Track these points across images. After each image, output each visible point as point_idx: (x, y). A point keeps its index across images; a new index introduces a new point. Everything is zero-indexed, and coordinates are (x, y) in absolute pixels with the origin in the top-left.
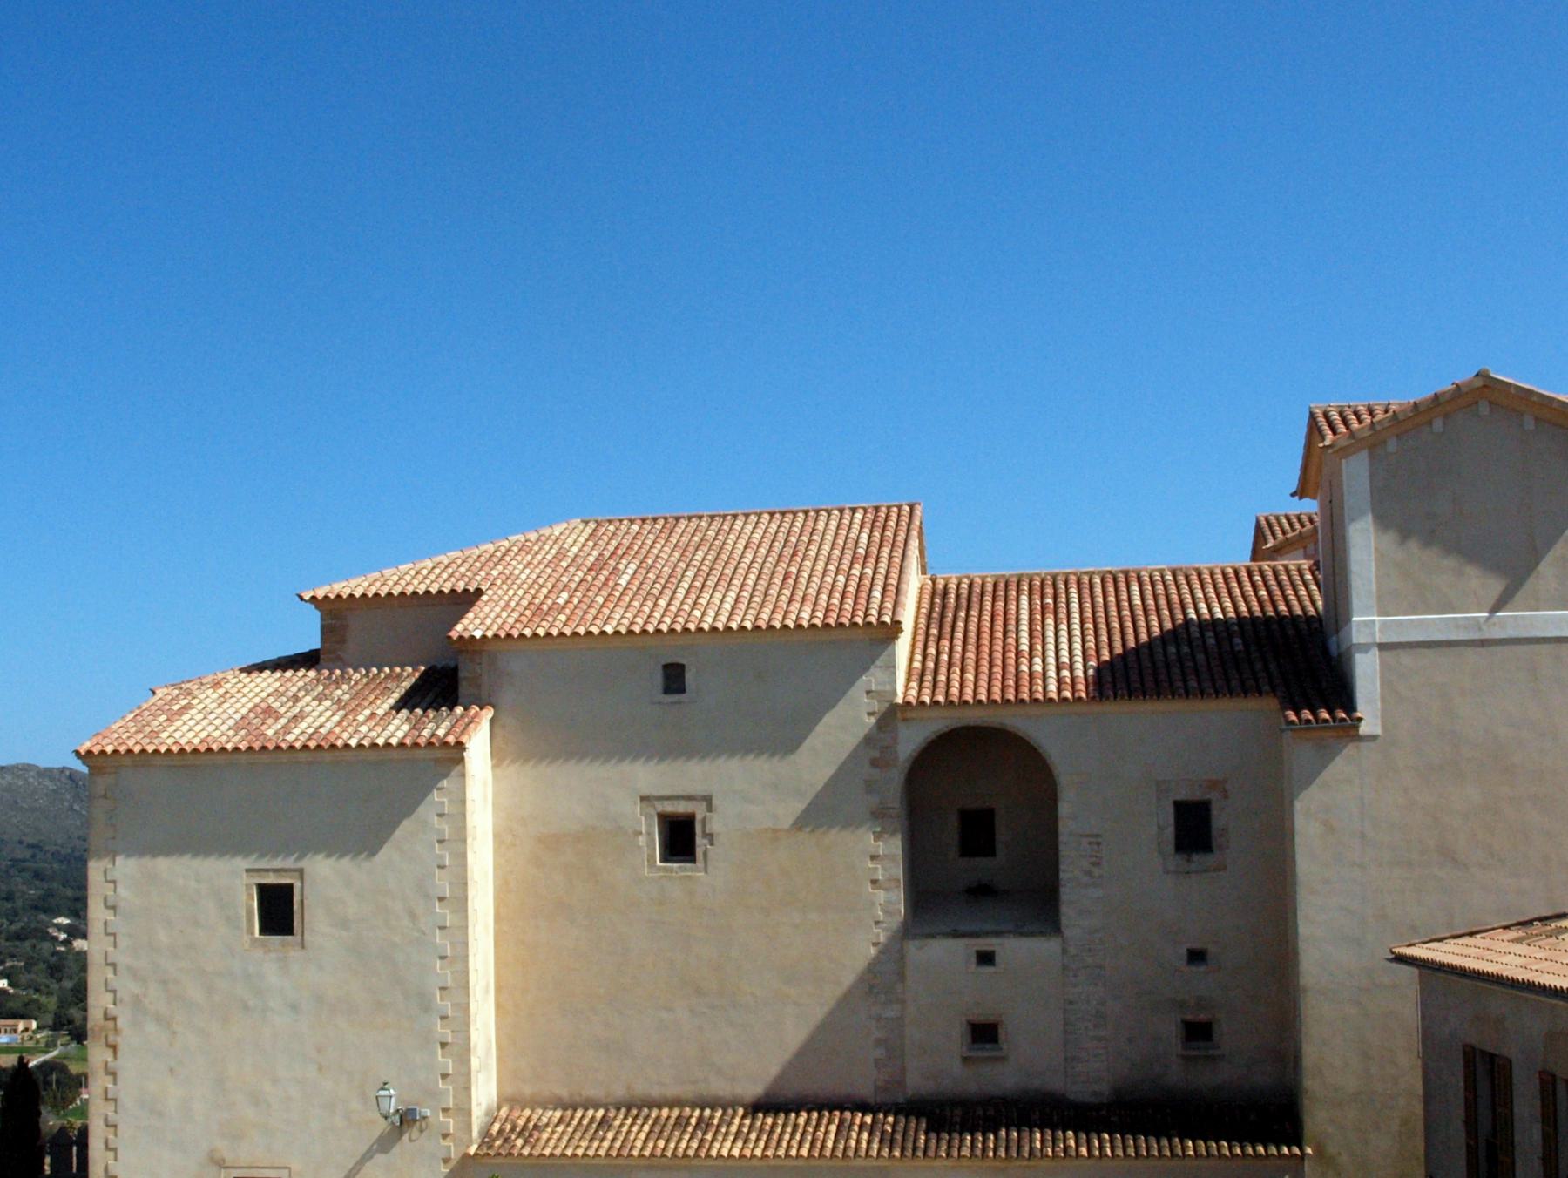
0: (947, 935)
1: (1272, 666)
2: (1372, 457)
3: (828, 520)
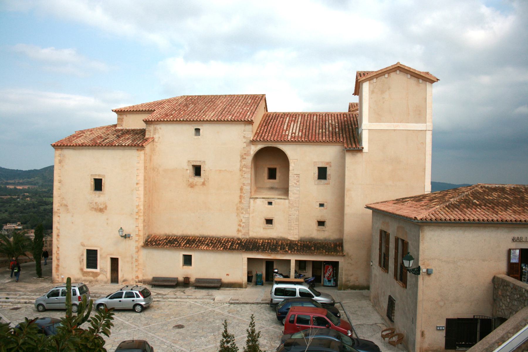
1: (344, 135)
2: (370, 83)
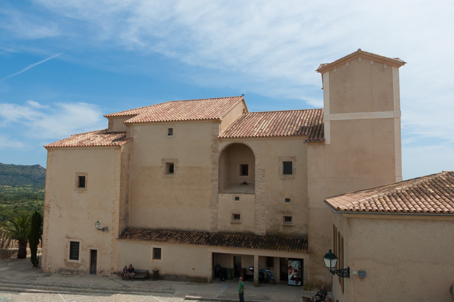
0: (228, 193)
2: (330, 73)
3: (292, 113)
